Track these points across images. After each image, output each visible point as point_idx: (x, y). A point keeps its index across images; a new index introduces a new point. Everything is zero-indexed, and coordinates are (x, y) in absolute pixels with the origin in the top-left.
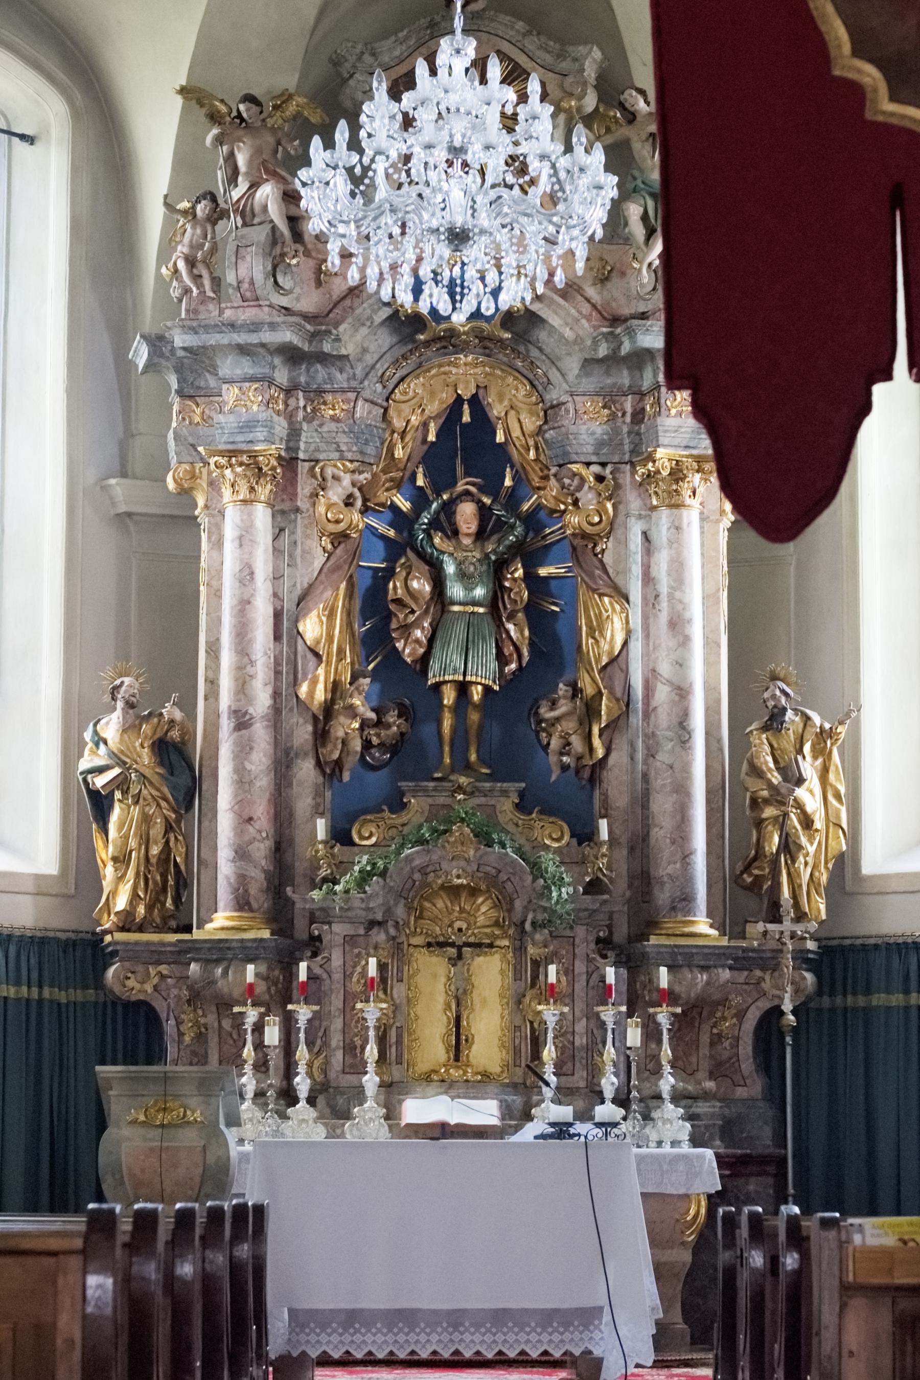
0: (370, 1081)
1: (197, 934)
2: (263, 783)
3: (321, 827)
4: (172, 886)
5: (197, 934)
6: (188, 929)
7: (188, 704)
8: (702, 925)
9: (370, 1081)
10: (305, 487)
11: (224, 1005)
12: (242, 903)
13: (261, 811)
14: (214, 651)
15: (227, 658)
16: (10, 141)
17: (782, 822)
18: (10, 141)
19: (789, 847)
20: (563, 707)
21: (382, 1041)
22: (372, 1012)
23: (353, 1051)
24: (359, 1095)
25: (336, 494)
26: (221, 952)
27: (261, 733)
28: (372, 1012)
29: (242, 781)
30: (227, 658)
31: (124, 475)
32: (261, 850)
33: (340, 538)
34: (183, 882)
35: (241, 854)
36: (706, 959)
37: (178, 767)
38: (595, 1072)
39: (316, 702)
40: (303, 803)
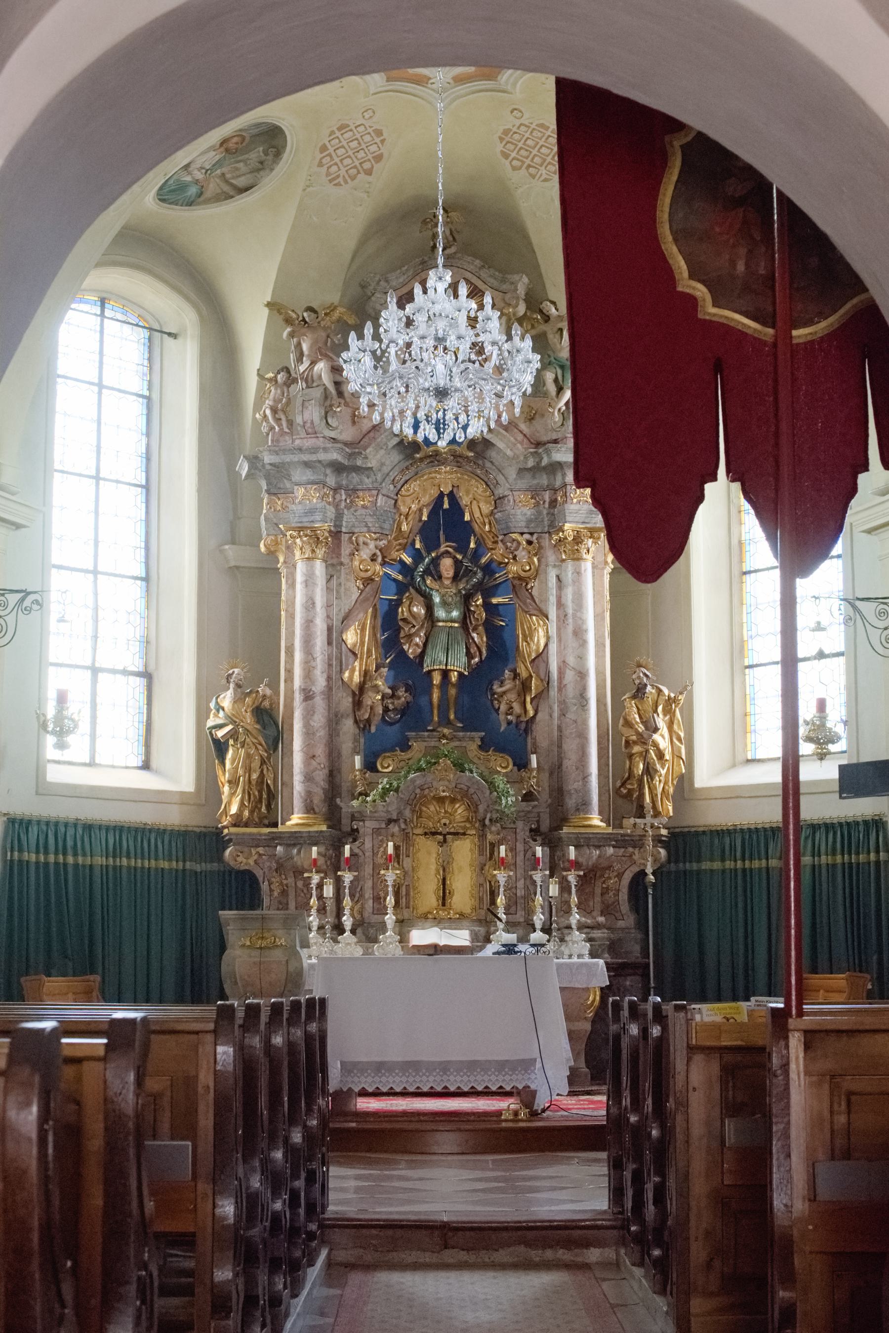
0: (390, 919)
1: (281, 828)
2: (322, 733)
3: (358, 761)
4: (265, 798)
5: (281, 828)
6: (275, 825)
8: (596, 820)
9: (390, 919)
10: (346, 549)
11: (298, 872)
12: (309, 809)
13: (320, 751)
15: (298, 656)
17: (645, 755)
19: (649, 771)
20: (508, 685)
21: (397, 894)
22: (390, 876)
23: (379, 900)
24: (383, 928)
25: (365, 554)
26: (296, 840)
27: (319, 702)
28: (390, 876)
29: (309, 733)
30: (298, 656)
32: (321, 776)
33: (368, 581)
34: (272, 796)
35: (308, 778)
37: (268, 724)
38: (530, 912)
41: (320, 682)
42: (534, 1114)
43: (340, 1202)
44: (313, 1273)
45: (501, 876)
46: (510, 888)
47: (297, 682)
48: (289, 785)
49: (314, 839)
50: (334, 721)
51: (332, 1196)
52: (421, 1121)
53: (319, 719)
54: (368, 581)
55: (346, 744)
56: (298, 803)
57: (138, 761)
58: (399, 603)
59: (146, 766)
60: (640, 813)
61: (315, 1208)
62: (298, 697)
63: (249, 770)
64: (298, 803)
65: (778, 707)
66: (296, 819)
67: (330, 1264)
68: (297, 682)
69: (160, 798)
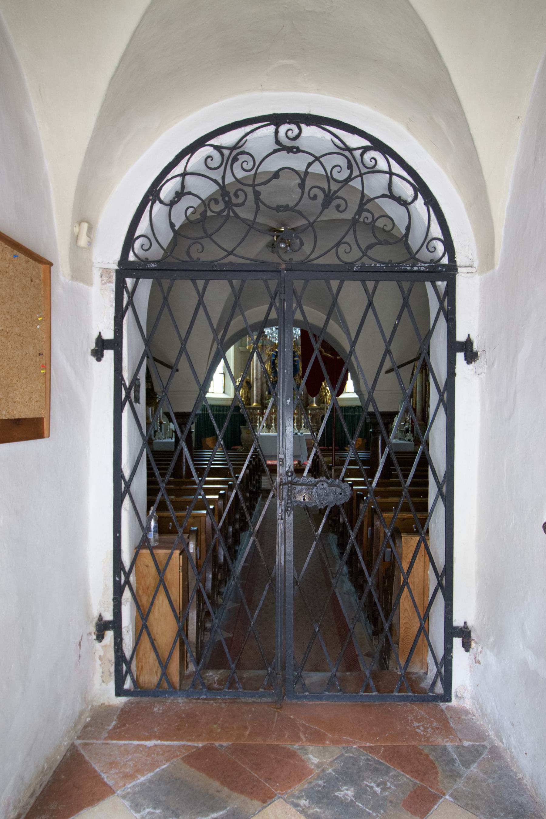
0: (273, 424)
1: (251, 406)
2: (260, 387)
3: (267, 393)
4: (249, 400)
5: (251, 406)
6: (250, 405)
7: (250, 377)
8: (315, 405)
9: (273, 424)
10: (264, 349)
11: (255, 415)
12: (257, 402)
13: (259, 391)
14: (253, 370)
15: (255, 371)
16: (226, 251)
17: (325, 392)
18: (226, 251)
19: (326, 395)
20: (297, 377)
21: (275, 420)
22: (273, 416)
23: (271, 421)
24: (272, 426)
25: (268, 350)
26: (254, 408)
27: (259, 381)
28: (273, 416)
29: (257, 387)
30: (255, 371)
31: (241, 346)
32: (260, 396)
33: (269, 355)
34: (250, 399)
35: (257, 396)
36: (315, 409)
37: (249, 385)
38: (301, 423)
39: (237, 292)
40: (265, 389)
41: (259, 376)
42: (300, 466)
43: (264, 485)
44: (259, 499)
45: (296, 417)
46: (297, 418)
47: (255, 377)
48: (253, 397)
49: (258, 409)
50: (262, 384)
51: (263, 484)
52: (262, 346)
53: (259, 384)
54: (269, 355)
55: (265, 389)
56: (255, 401)
57: (223, 391)
58: (275, 359)
59: (224, 392)
60: (324, 403)
61: (260, 487)
62: (255, 380)
63: (245, 394)
64: (255, 401)
65: (378, 313)
66: (254, 404)
67: (262, 497)
68: (255, 377)
69: (227, 399)
